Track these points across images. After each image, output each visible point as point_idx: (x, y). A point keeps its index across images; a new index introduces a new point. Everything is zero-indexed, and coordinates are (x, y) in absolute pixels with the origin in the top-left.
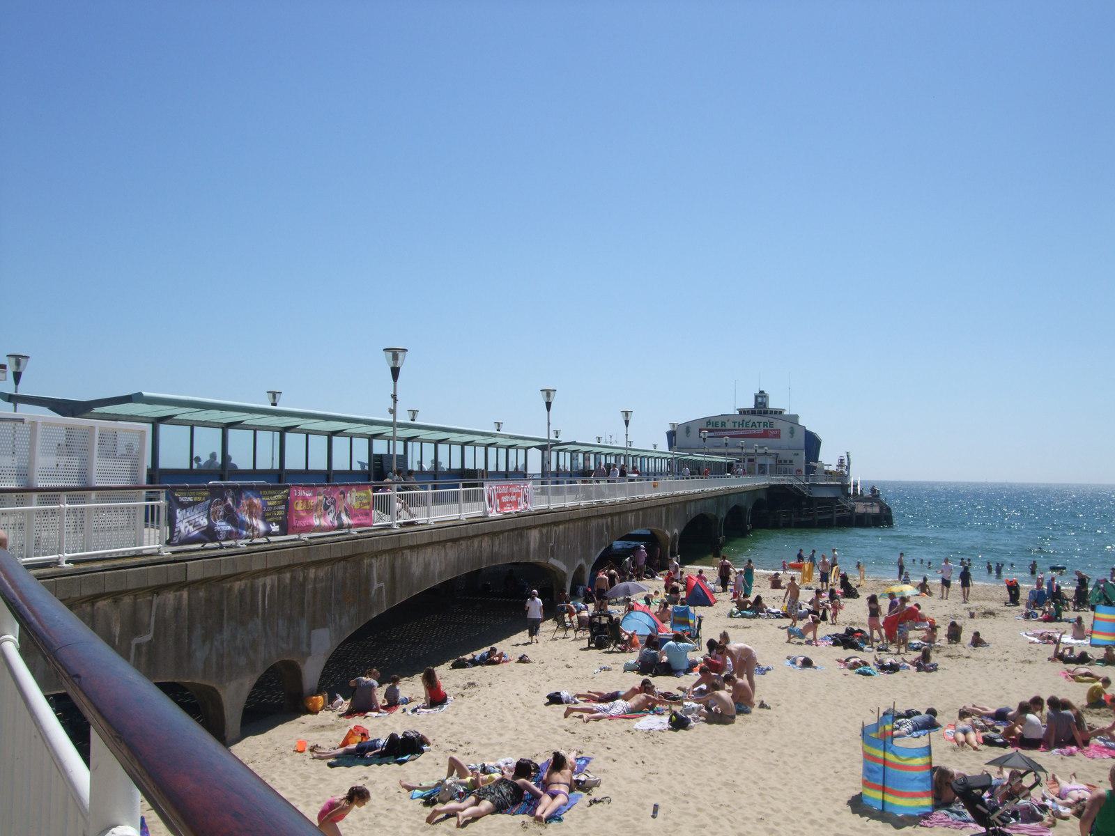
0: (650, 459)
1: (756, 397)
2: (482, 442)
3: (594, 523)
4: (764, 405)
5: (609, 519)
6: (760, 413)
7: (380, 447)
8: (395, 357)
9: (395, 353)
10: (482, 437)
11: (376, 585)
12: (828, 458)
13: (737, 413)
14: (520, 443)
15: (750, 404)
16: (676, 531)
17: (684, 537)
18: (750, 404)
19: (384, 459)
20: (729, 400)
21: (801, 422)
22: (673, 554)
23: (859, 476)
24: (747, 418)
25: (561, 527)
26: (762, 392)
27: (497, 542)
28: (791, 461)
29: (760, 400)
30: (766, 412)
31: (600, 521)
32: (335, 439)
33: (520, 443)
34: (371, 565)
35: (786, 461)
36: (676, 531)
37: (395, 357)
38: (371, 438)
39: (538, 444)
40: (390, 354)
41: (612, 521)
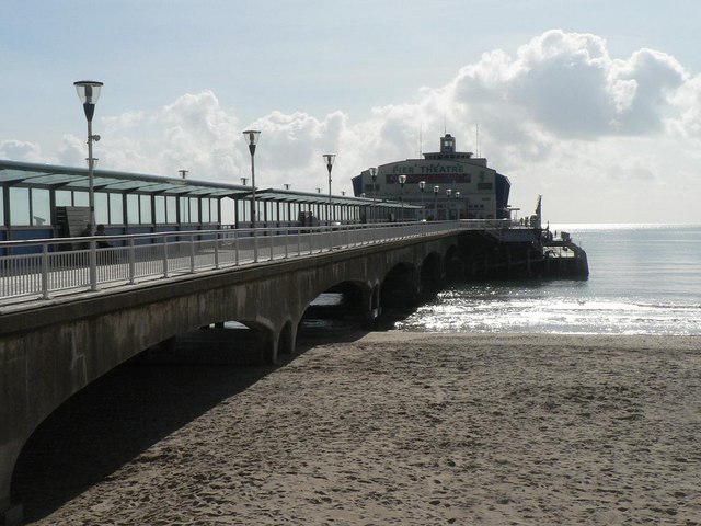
0: (292, 204)
1: (443, 140)
2: (147, 189)
3: (300, 275)
4: (452, 148)
5: (314, 272)
6: (447, 157)
7: (63, 199)
8: (89, 93)
9: (88, 87)
10: (147, 184)
11: (76, 357)
12: (520, 206)
13: (423, 158)
14: (142, 185)
15: (437, 149)
16: (377, 281)
17: (384, 287)
18: (437, 149)
19: (68, 213)
20: (420, 145)
21: (489, 165)
22: (374, 307)
23: (554, 225)
24: (435, 162)
25: (268, 282)
26: (448, 136)
27: (203, 302)
28: (482, 206)
29: (446, 144)
30: (453, 157)
31: (304, 273)
32: (12, 190)
33: (142, 185)
34: (70, 334)
35: (476, 206)
36: (377, 281)
37: (89, 93)
38: (53, 188)
39: (231, 192)
40: (83, 89)
41: (317, 274)
